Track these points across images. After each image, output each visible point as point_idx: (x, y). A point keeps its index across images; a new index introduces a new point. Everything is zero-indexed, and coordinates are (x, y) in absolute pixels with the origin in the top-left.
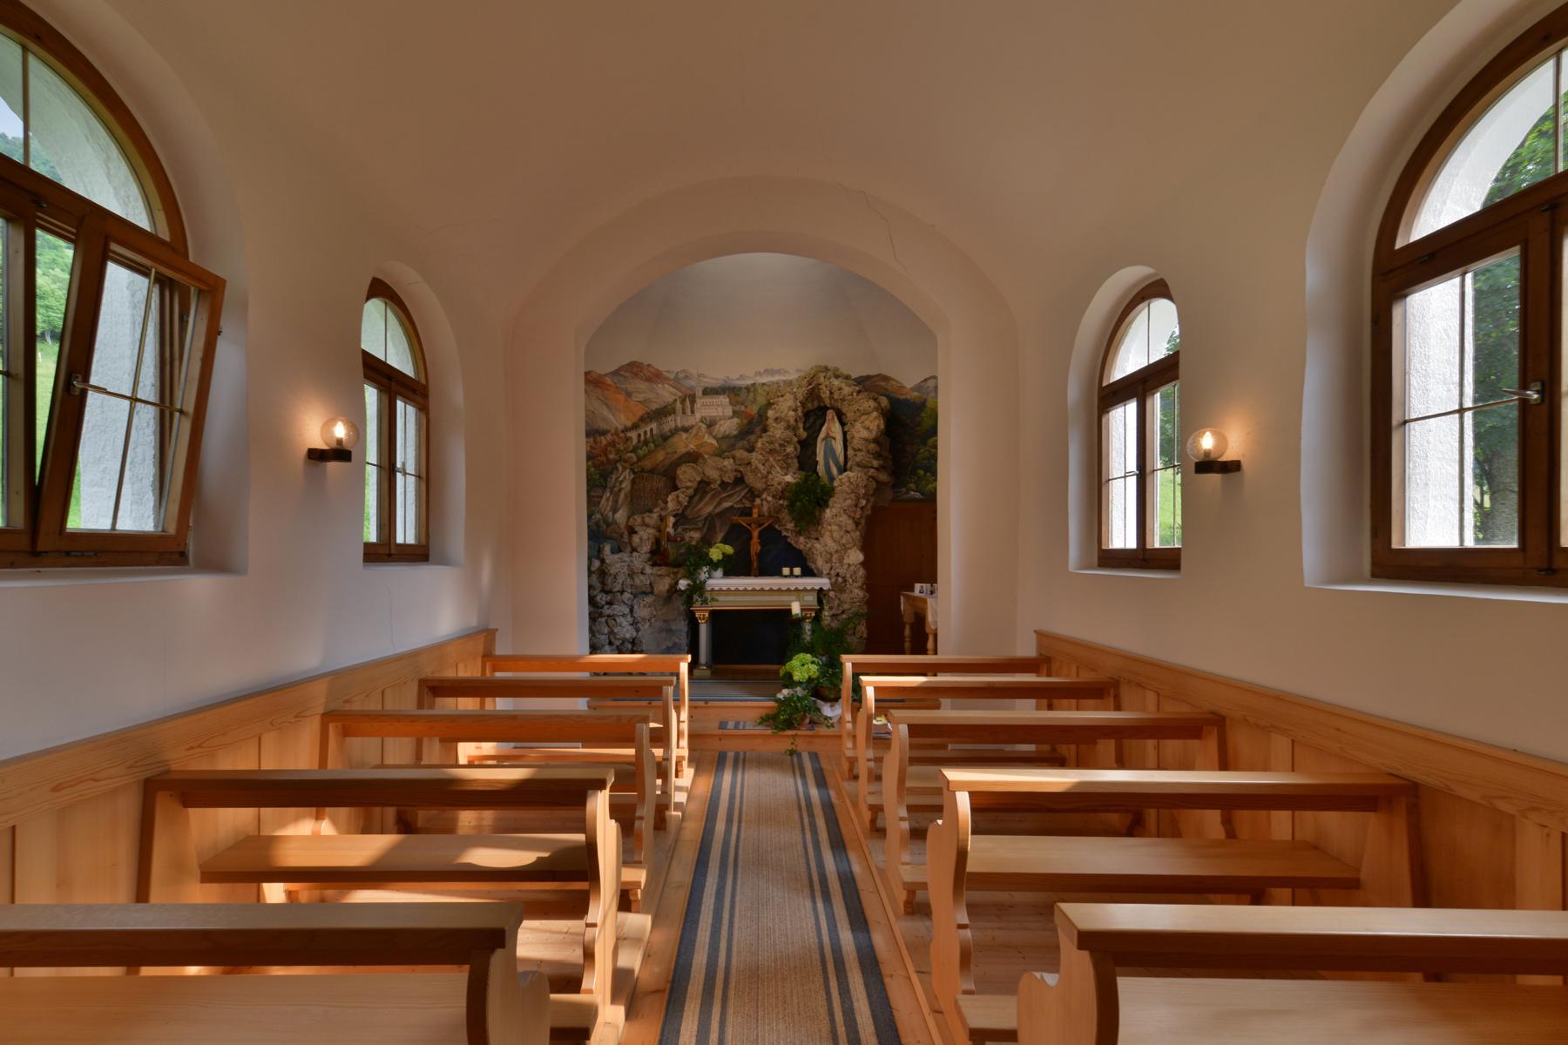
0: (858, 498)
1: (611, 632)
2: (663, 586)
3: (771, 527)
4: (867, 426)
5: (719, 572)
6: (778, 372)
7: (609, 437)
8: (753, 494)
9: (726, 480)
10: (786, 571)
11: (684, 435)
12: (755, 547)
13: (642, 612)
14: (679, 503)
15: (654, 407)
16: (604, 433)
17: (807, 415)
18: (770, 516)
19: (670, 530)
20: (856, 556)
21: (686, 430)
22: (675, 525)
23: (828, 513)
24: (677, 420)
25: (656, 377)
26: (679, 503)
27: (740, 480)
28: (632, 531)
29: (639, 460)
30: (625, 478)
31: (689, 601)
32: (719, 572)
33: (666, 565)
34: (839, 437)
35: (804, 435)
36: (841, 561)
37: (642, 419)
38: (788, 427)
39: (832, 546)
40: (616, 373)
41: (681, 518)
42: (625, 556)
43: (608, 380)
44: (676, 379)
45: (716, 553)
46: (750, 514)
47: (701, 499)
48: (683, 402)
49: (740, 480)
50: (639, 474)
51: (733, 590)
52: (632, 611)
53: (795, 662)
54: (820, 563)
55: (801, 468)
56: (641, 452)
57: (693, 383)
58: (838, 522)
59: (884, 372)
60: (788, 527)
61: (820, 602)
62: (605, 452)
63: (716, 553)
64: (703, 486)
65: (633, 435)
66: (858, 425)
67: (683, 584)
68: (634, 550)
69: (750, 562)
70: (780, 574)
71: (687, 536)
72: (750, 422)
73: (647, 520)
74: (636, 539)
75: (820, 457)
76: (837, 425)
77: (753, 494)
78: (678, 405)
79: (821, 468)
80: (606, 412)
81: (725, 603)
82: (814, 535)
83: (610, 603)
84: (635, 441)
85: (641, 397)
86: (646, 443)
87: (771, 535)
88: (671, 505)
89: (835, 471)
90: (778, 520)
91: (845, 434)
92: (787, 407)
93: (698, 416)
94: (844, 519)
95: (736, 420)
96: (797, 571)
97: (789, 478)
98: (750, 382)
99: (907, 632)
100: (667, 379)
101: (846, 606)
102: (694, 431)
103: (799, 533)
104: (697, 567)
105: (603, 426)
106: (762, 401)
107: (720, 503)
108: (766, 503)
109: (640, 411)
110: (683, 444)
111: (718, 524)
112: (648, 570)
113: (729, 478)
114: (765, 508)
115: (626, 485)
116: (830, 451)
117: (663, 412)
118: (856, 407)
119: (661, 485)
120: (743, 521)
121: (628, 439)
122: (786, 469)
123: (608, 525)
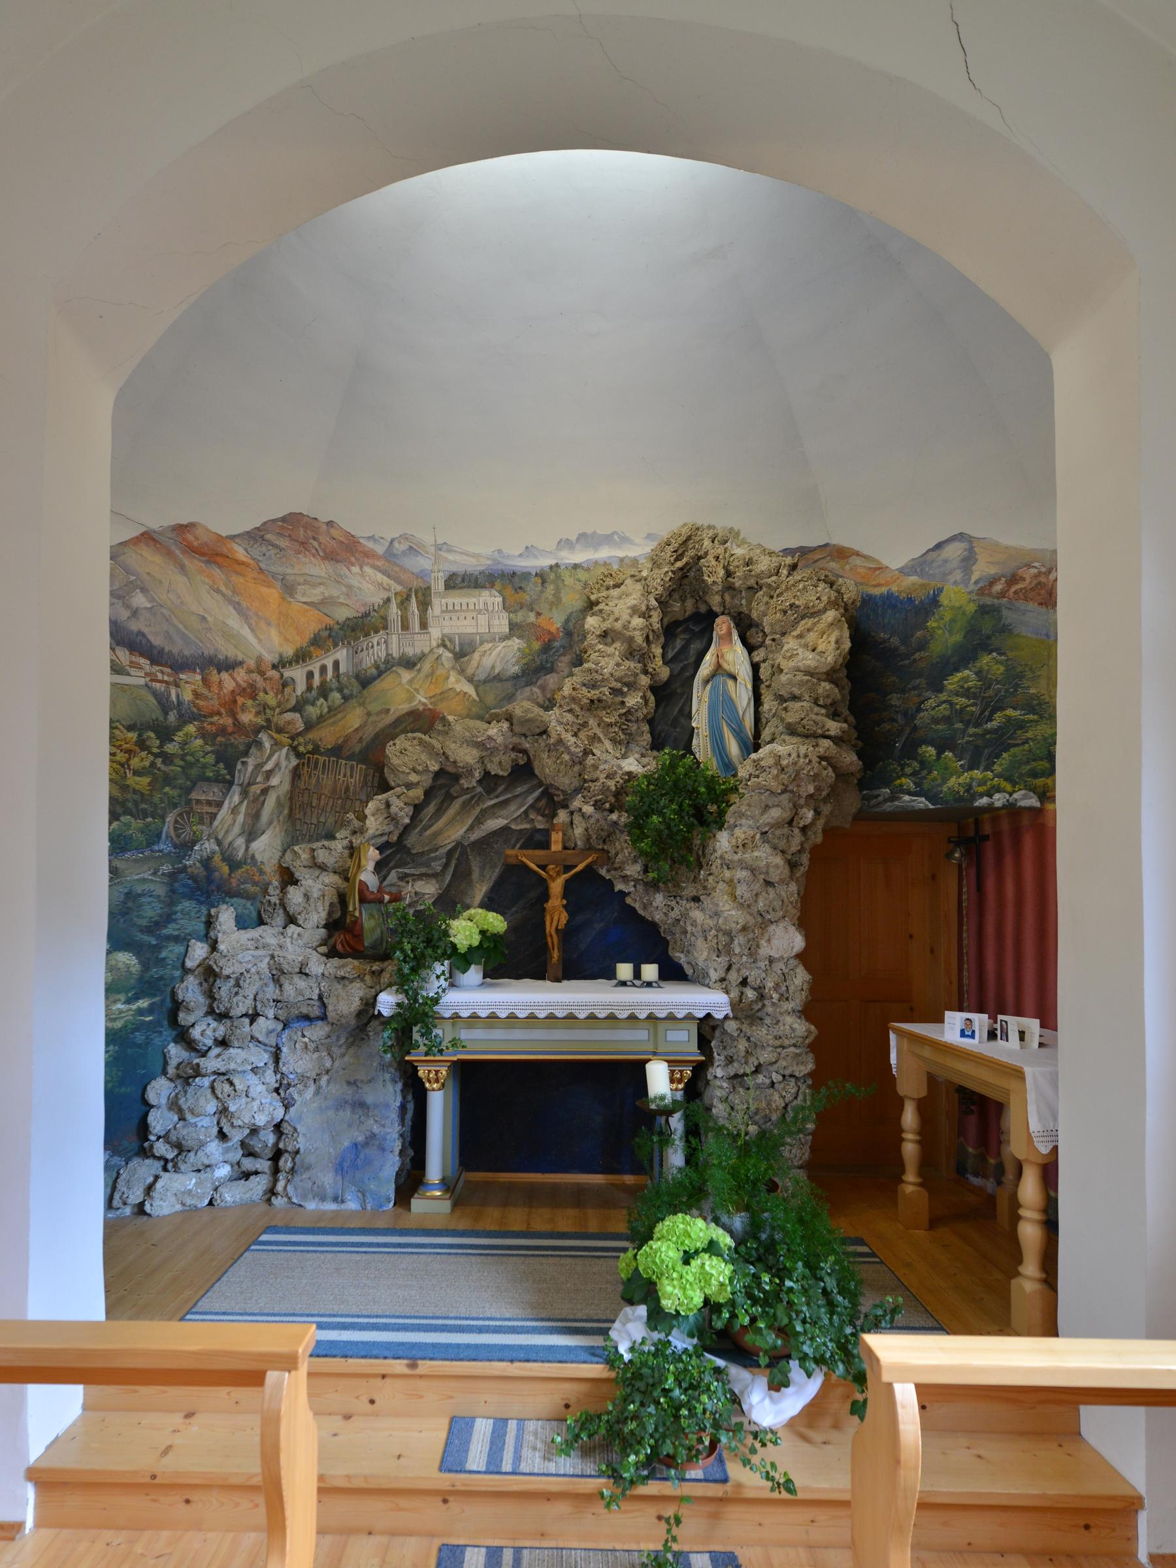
0: (796, 807)
1: (224, 1111)
2: (346, 1002)
3: (590, 870)
4: (816, 646)
5: (474, 975)
6: (608, 540)
7: (241, 675)
8: (552, 801)
9: (494, 769)
10: (624, 970)
11: (406, 675)
12: (556, 915)
13: (297, 1062)
14: (392, 818)
15: (342, 614)
16: (229, 666)
17: (670, 630)
18: (589, 848)
19: (367, 876)
20: (787, 940)
21: (409, 663)
22: (380, 867)
23: (723, 842)
24: (395, 644)
25: (346, 550)
26: (392, 818)
27: (523, 771)
28: (288, 878)
29: (309, 726)
30: (276, 765)
31: (403, 1040)
32: (474, 975)
33: (356, 954)
34: (744, 671)
35: (664, 673)
36: (752, 951)
37: (316, 641)
38: (630, 654)
39: (733, 916)
40: (256, 536)
41: (394, 853)
42: (268, 934)
43: (239, 552)
44: (390, 555)
45: (464, 931)
46: (545, 845)
47: (440, 812)
48: (404, 603)
49: (523, 771)
50: (308, 759)
51: (492, 1011)
52: (277, 1057)
53: (663, 1250)
54: (701, 954)
55: (657, 745)
56: (312, 711)
57: (422, 563)
58: (745, 849)
59: (840, 539)
60: (628, 872)
61: (704, 1043)
62: (231, 707)
63: (464, 931)
64: (444, 784)
65: (297, 674)
66: (790, 643)
67: (387, 1002)
68: (291, 920)
69: (544, 949)
70: (610, 974)
71: (408, 890)
72: (547, 648)
73: (322, 856)
74: (295, 895)
75: (700, 719)
76: (739, 647)
77: (552, 801)
78: (394, 611)
79: (701, 745)
80: (234, 622)
81: (483, 1045)
82: (690, 890)
83: (223, 1043)
84: (301, 687)
85: (316, 594)
86: (324, 691)
87: (589, 889)
88: (374, 824)
89: (733, 748)
90: (607, 858)
91: (755, 667)
92: (628, 609)
93: (435, 633)
94: (763, 855)
95: (516, 643)
96: (650, 971)
97: (631, 764)
98: (545, 562)
99: (909, 1117)
100: (369, 554)
101: (765, 1056)
102: (426, 666)
103: (653, 886)
104: (419, 964)
105: (227, 650)
106: (572, 600)
107: (479, 821)
108: (580, 820)
109: (312, 624)
110: (402, 694)
111: (475, 865)
112: (317, 966)
113: (499, 766)
114: (578, 831)
115: (280, 782)
116: (722, 706)
117: (360, 627)
118: (787, 599)
119: (355, 780)
120: (530, 859)
121: (285, 684)
122: (625, 743)
123: (234, 865)
